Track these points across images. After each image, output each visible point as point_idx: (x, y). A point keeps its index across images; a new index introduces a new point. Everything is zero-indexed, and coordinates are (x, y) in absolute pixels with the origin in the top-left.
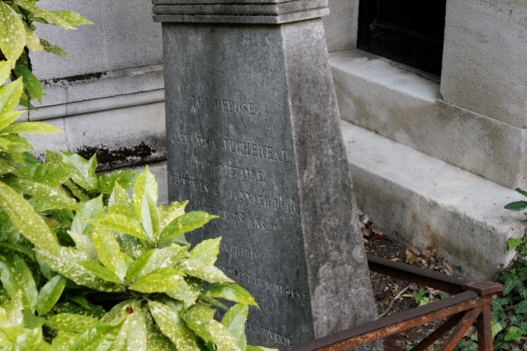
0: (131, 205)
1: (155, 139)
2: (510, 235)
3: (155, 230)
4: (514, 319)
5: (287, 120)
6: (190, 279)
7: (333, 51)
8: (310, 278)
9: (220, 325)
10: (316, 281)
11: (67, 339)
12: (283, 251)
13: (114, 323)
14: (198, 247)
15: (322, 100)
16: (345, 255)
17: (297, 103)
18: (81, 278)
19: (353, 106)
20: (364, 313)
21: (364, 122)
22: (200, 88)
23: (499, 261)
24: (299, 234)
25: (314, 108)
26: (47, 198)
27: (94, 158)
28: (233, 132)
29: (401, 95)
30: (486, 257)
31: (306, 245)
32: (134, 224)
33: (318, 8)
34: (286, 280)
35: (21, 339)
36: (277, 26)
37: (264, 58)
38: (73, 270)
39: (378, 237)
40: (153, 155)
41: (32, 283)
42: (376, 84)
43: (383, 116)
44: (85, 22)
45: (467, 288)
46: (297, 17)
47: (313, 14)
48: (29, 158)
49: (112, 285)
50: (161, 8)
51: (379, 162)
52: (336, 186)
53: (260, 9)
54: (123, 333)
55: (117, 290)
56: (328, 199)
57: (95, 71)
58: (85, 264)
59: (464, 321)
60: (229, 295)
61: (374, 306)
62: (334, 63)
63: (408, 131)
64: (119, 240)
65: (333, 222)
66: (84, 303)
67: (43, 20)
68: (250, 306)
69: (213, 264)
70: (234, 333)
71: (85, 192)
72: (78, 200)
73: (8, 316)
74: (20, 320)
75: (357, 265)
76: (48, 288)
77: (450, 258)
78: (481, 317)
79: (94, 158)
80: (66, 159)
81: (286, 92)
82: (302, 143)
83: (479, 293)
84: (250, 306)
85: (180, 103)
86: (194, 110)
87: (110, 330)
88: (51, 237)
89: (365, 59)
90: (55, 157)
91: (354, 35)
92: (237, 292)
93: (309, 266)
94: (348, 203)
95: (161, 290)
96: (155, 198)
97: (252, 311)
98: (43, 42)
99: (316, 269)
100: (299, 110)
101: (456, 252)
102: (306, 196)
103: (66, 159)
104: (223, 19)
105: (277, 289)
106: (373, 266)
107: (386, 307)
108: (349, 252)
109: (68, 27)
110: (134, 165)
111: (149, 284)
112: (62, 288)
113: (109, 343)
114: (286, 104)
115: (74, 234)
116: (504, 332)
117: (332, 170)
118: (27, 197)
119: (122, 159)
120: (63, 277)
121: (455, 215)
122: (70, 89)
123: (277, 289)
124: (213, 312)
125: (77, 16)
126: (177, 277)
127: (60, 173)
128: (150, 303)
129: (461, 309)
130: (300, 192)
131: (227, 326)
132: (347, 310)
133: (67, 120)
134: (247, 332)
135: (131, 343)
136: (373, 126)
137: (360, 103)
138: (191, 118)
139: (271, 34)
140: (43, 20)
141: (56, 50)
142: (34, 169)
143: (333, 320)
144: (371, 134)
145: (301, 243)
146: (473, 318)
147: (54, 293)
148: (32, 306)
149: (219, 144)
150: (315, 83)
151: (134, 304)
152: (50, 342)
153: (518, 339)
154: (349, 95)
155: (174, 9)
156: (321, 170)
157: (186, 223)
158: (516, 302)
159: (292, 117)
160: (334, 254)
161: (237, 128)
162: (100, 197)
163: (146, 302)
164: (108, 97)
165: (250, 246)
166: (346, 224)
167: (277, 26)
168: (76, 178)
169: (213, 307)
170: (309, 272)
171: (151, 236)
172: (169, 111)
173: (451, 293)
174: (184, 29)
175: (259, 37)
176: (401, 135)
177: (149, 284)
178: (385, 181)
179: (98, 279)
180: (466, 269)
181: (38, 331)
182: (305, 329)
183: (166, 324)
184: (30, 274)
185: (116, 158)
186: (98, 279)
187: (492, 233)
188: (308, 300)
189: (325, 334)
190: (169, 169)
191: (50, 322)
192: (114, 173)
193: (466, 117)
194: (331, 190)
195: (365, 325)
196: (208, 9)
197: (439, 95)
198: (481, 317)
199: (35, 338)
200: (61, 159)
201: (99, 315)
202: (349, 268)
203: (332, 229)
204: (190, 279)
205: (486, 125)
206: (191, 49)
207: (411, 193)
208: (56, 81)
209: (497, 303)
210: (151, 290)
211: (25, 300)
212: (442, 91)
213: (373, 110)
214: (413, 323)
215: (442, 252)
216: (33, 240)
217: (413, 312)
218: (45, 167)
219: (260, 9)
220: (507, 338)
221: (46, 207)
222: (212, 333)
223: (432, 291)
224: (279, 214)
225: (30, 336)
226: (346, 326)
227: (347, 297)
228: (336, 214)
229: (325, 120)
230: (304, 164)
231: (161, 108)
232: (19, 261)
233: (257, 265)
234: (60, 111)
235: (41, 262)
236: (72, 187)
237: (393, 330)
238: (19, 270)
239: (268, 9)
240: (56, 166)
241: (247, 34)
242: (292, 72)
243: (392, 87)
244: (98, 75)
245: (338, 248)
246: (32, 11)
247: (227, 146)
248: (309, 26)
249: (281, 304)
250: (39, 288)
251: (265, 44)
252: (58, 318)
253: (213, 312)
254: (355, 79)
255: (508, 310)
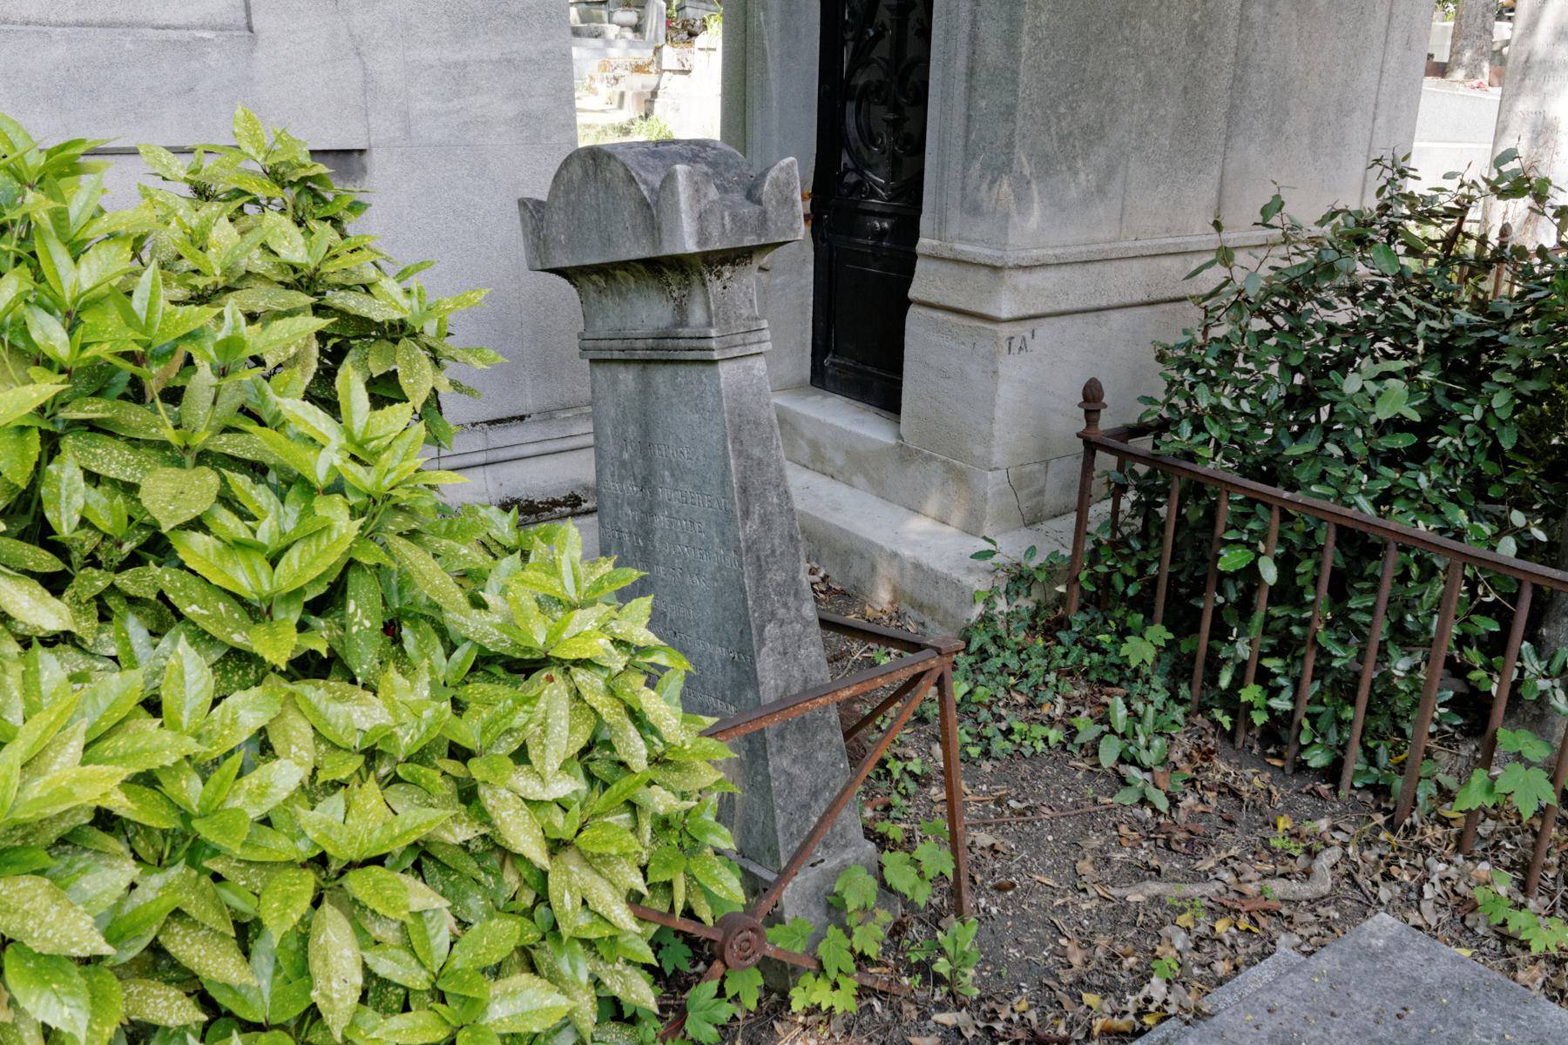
0: (553, 562)
1: (587, 489)
2: (977, 587)
3: (577, 589)
4: (981, 678)
5: (727, 465)
6: (619, 643)
7: (784, 389)
8: (755, 639)
9: (653, 693)
10: (762, 642)
11: (480, 713)
12: (725, 609)
13: (531, 694)
14: (627, 609)
15: (765, 443)
16: (793, 613)
17: (738, 446)
18: (495, 644)
19: (806, 449)
20: (816, 676)
21: (819, 466)
22: (632, 431)
23: (966, 616)
24: (742, 590)
25: (757, 452)
26: (457, 557)
27: (515, 510)
28: (668, 479)
29: (858, 436)
30: (951, 611)
31: (750, 603)
32: (554, 581)
33: (759, 342)
34: (729, 641)
35: (427, 714)
36: (713, 362)
37: (700, 397)
38: (485, 635)
39: (836, 592)
40: (585, 506)
41: (440, 651)
42: (831, 425)
43: (839, 459)
44: (500, 359)
45: (927, 646)
46: (736, 352)
47: (754, 349)
48: (443, 510)
49: (530, 650)
50: (589, 344)
51: (836, 510)
52: (782, 537)
53: (695, 343)
54: (542, 705)
55: (536, 657)
56: (773, 551)
57: (518, 414)
58: (500, 627)
59: (923, 682)
60: (661, 659)
61: (825, 668)
62: (779, 400)
63: (867, 475)
64: (538, 600)
65: (779, 577)
66: (498, 671)
67: (452, 358)
68: (687, 672)
69: (105, 805)
70: (668, 700)
71: (505, 548)
72: (495, 557)
73: (412, 689)
74: (426, 693)
75: (807, 624)
76: (457, 655)
77: (913, 613)
78: (941, 678)
79: (515, 510)
80: (482, 512)
81: (725, 435)
82: (744, 490)
83: (939, 651)
84: (687, 672)
85: (610, 448)
86: (626, 456)
87: (527, 701)
88: (460, 597)
89: (819, 398)
90: (472, 511)
91: (807, 372)
92: (671, 659)
93: (753, 626)
94: (796, 555)
95: (584, 656)
96: (578, 554)
97: (689, 679)
98: (452, 383)
99: (761, 629)
100: (740, 454)
101: (920, 607)
102: (749, 549)
103: (482, 512)
104: (655, 355)
105: (719, 652)
106: (825, 624)
107: (844, 668)
108: (798, 610)
109: (480, 365)
110: (563, 517)
111: (571, 649)
112: (474, 655)
113: (526, 717)
114: (726, 448)
115: (487, 596)
116: (970, 692)
117: (778, 520)
118: (435, 556)
119: (549, 510)
120: (475, 643)
121: (917, 566)
122: (490, 433)
123: (719, 652)
124: (644, 678)
125: (492, 354)
126: (604, 642)
127: (474, 528)
128: (573, 670)
129: (919, 669)
130: (743, 544)
131: (661, 694)
132: (796, 673)
133: (488, 468)
134: (683, 697)
135: (552, 714)
136: (829, 470)
137: (814, 445)
138: (623, 464)
139: (708, 369)
140: (452, 358)
141: (470, 392)
142: (445, 524)
143: (781, 684)
144: (827, 479)
145: (745, 600)
146: (935, 676)
147: (465, 661)
148: (440, 675)
149: (654, 493)
150: (757, 424)
151: (554, 672)
152: (459, 715)
153: (986, 700)
154: (802, 437)
155: (603, 344)
156: (765, 521)
157: (611, 580)
158: (984, 660)
159: (732, 462)
160: (781, 612)
161: (673, 475)
162: (518, 554)
163: (568, 669)
164: (1085, 311)
165: (689, 604)
166: (794, 579)
167: (713, 362)
168: (494, 533)
169: (645, 672)
170: (754, 632)
171: (573, 595)
172: (599, 457)
173: (912, 652)
174: (614, 366)
175: (695, 375)
176: (859, 480)
177: (571, 649)
178: (842, 530)
179: (515, 644)
180: (931, 625)
181: (446, 706)
182: (750, 695)
183: (591, 691)
184: (437, 641)
185: (543, 510)
186: (515, 644)
187: (956, 585)
188: (753, 662)
189: (773, 699)
190: (601, 521)
191: (461, 694)
192: (538, 527)
193: (929, 459)
194: (777, 542)
195: (816, 689)
196: (639, 344)
197: (900, 437)
198: (941, 678)
199: (443, 713)
200: (477, 512)
201: (516, 685)
202: (798, 627)
203: (778, 585)
204: (619, 643)
205: (950, 469)
206: (622, 388)
207: (871, 544)
208: (473, 425)
209: (964, 661)
210: (573, 656)
211: (432, 670)
212: (903, 431)
213: (829, 453)
214: (868, 687)
215: (904, 607)
216: (440, 601)
217: (873, 672)
218: (458, 521)
219: (695, 343)
220: (974, 699)
221: (458, 566)
222: (644, 701)
223: (894, 651)
224: (720, 568)
225: (437, 711)
226: (795, 690)
227: (796, 659)
228: (782, 568)
229: (769, 465)
230: (746, 514)
231: (591, 453)
232: (425, 626)
233: (697, 625)
234: (480, 458)
235: (450, 627)
236: (490, 544)
237: (846, 693)
238: (425, 636)
239: (703, 343)
240: (470, 520)
241: (682, 370)
242: (731, 413)
243: (849, 428)
244: (522, 418)
245: (785, 605)
246: (440, 348)
247: (663, 494)
248: (749, 362)
249: (724, 667)
250: (448, 657)
251: (701, 382)
252: (470, 689)
253: (644, 678)
254: (809, 419)
255: (974, 669)
